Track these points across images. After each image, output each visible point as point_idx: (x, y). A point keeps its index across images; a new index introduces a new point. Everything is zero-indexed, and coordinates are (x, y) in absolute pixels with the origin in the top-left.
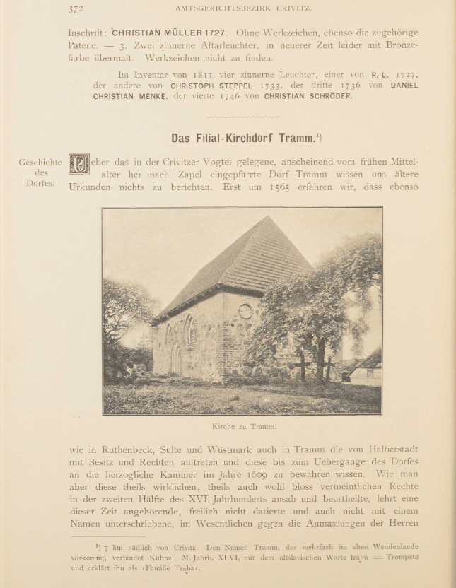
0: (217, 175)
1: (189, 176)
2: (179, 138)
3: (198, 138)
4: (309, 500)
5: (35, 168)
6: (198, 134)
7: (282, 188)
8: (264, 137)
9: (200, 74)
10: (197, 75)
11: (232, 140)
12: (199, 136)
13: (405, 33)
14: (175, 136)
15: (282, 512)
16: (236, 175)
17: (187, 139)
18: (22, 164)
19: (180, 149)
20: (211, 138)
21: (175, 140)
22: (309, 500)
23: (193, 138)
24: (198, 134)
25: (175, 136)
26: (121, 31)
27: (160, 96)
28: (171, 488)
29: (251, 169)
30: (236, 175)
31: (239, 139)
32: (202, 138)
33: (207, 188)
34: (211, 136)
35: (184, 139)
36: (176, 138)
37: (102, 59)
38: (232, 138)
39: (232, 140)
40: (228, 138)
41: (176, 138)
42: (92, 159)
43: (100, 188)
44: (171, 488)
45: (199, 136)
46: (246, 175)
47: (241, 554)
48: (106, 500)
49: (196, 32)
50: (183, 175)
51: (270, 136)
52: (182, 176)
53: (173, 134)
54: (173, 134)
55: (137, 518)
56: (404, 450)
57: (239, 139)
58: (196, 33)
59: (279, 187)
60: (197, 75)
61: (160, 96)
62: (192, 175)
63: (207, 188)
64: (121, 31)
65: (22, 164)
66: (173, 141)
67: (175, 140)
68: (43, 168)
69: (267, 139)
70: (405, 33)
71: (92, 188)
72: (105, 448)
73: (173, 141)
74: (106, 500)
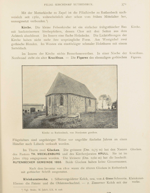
0: (38, 58)
1: (62, 13)
13: (50, 140)
16: (52, 32)
26: (34, 154)
27: (31, 162)
29: (106, 42)
30: (52, 32)
33: (68, 144)
43: (34, 44)
46: (26, 140)
47: (96, 15)
48: (41, 150)
49: (33, 162)
50: (60, 13)
52: (60, 13)
55: (43, 142)
58: (33, 162)
59: (26, 158)
61: (31, 162)
62: (63, 13)
63: (68, 144)
64: (34, 154)
70: (50, 140)
71: (39, 21)
72: (102, 12)
74: (41, 150)
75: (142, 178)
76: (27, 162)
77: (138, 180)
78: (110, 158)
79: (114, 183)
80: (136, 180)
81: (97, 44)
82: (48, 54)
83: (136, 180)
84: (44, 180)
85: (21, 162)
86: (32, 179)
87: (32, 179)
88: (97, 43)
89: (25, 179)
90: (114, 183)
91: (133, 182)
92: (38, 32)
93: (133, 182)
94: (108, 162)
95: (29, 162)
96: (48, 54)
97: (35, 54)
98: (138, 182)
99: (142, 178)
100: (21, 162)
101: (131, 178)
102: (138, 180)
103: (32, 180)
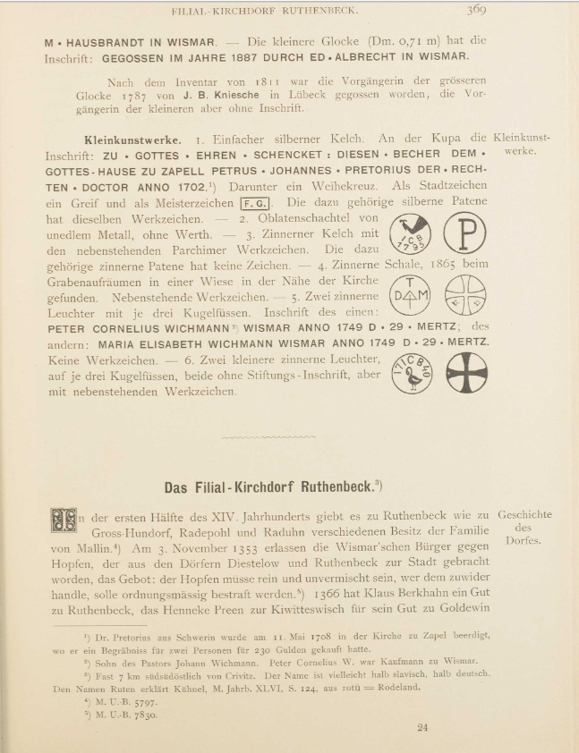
2: (173, 488)
3: (197, 487)
4: (298, 564)
5: (516, 522)
6: (197, 483)
7: (446, 264)
8: (283, 486)
9: (264, 81)
10: (260, 82)
11: (243, 489)
12: (199, 485)
14: (169, 485)
15: (275, 564)
17: (184, 490)
18: (401, 610)
19: (175, 502)
20: (214, 488)
21: (169, 490)
22: (298, 564)
23: (191, 487)
24: (197, 483)
25: (169, 485)
27: (308, 154)
28: (422, 594)
31: (251, 489)
32: (203, 487)
34: (214, 485)
35: (180, 489)
36: (170, 488)
37: (110, 612)
38: (242, 487)
39: (243, 489)
40: (237, 487)
41: (170, 488)
42: (79, 514)
44: (422, 594)
45: (199, 485)
51: (290, 485)
53: (166, 483)
54: (166, 483)
56: (419, 563)
57: (251, 489)
60: (260, 82)
61: (308, 154)
65: (401, 610)
66: (166, 492)
67: (169, 490)
68: (524, 522)
69: (286, 489)
73: (166, 492)
75: (545, 138)
76: (466, 167)
77: (528, 145)
78: (76, 221)
79: (341, 610)
80: (518, 145)
81: (185, 581)
82: (352, 282)
83: (518, 145)
84: (164, 141)
85: (230, 153)
86: (120, 141)
87: (120, 141)
88: (185, 577)
89: (92, 140)
90: (341, 610)
91: (508, 152)
92: (374, 297)
93: (508, 152)
94: (444, 609)
95: (301, 155)
96: (352, 282)
97: (296, 235)
98: (527, 152)
99: (545, 138)
100: (230, 153)
101: (501, 137)
102: (528, 145)
103: (117, 142)
